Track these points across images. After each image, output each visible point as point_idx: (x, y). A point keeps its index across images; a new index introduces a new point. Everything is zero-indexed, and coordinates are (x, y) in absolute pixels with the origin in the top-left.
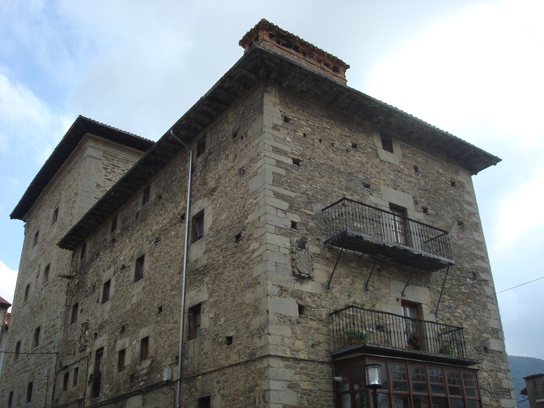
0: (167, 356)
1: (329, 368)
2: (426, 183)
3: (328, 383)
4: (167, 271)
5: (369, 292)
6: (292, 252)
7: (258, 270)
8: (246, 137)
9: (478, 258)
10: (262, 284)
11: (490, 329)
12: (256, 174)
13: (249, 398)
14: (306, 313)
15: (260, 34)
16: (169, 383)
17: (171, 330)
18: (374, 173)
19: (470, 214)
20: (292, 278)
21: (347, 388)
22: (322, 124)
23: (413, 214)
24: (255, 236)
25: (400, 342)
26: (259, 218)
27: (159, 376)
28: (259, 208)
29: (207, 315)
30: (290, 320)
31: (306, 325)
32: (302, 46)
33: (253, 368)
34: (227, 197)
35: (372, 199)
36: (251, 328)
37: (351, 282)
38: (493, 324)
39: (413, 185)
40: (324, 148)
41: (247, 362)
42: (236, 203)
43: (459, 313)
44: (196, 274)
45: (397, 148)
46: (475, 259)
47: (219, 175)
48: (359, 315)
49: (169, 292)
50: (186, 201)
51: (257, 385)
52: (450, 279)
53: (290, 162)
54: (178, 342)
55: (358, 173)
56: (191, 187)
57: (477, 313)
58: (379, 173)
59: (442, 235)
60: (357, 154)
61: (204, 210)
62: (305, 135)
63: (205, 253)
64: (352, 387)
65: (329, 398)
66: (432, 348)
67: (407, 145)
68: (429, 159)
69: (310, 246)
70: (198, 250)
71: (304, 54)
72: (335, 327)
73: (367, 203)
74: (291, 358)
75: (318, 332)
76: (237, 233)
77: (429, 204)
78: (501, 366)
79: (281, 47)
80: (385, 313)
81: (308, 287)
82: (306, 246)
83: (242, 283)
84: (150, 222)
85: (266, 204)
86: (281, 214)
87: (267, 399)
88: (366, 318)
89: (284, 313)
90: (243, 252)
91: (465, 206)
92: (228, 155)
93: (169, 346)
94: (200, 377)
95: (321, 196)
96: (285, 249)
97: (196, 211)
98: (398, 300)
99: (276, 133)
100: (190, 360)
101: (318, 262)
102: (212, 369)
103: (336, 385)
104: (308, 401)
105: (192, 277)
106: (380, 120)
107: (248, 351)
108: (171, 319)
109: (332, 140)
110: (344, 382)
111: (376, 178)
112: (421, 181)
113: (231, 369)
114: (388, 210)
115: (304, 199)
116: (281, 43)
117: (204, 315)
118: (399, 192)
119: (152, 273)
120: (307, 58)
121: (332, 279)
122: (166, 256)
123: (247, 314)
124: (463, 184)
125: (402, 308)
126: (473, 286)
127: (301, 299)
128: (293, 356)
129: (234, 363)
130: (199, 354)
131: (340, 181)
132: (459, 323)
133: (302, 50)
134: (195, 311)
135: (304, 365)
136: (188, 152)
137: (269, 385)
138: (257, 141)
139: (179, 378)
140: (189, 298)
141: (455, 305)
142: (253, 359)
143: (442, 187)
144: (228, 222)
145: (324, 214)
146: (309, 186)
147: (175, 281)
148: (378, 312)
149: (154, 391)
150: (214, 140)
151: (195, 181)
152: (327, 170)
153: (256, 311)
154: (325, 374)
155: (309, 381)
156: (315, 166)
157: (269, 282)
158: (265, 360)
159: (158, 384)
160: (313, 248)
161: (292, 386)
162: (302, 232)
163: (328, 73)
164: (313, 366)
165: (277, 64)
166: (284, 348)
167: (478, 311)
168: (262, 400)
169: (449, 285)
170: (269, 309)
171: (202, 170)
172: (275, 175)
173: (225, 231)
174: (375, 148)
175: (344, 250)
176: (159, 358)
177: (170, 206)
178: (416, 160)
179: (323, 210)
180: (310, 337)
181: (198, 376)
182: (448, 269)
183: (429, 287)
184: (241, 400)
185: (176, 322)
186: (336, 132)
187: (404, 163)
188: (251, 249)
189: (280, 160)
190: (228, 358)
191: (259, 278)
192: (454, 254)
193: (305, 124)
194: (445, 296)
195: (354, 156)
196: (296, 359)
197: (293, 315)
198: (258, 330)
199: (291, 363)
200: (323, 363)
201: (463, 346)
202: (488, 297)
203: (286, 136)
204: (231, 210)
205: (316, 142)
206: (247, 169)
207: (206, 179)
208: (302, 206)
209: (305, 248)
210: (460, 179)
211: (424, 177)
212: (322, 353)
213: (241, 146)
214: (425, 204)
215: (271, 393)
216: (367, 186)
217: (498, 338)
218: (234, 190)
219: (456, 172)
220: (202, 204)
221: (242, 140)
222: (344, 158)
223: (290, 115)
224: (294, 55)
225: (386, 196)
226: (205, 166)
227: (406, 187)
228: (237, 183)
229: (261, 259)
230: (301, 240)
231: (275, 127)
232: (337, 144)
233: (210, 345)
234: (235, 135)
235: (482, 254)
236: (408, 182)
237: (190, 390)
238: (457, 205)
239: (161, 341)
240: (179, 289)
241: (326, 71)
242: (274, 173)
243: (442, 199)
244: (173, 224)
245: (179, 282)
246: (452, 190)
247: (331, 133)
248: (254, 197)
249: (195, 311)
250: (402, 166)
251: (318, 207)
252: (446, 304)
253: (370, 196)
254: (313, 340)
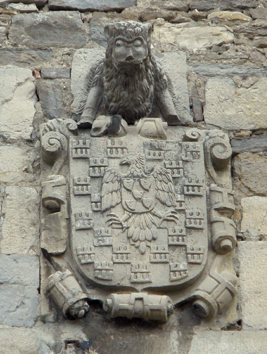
20: (45, 336)
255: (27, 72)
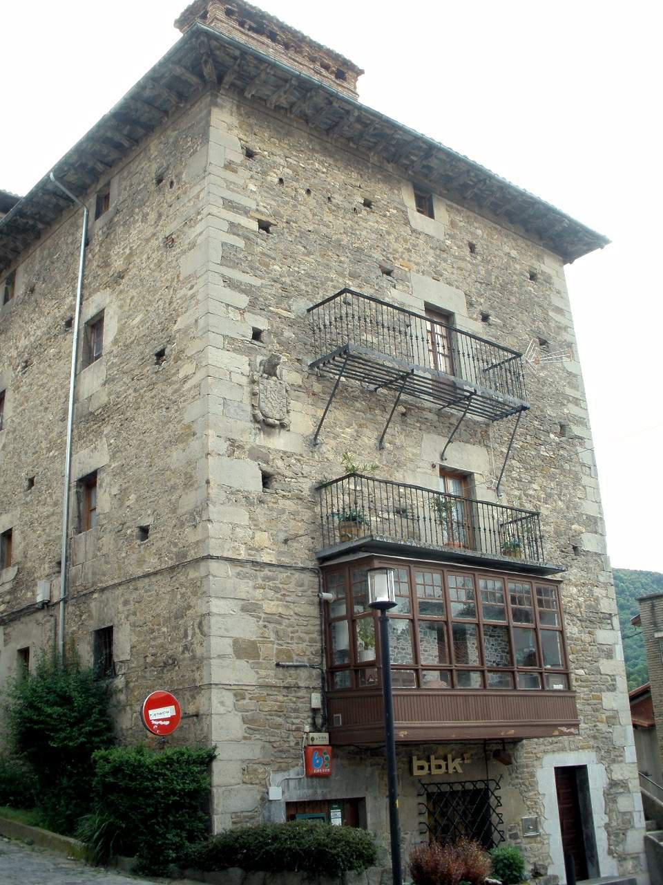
0: (42, 560)
1: (312, 579)
2: (489, 273)
3: (312, 604)
4: (43, 417)
5: (385, 452)
6: (253, 382)
7: (192, 412)
8: (178, 183)
9: (569, 401)
10: (198, 435)
11: (584, 517)
12: (193, 245)
13: (177, 628)
14: (275, 484)
15: (210, 8)
16: (46, 605)
17: (48, 517)
18: (400, 250)
19: (559, 328)
20: (252, 425)
21: (343, 611)
22: (312, 164)
23: (463, 321)
24: (189, 353)
25: (434, 536)
26: (196, 321)
27: (29, 594)
28: (197, 303)
29: (108, 489)
30: (246, 497)
31: (275, 506)
32: (284, 32)
33: (182, 579)
34: (143, 285)
35: (394, 295)
36: (180, 511)
37: (355, 434)
38: (588, 508)
39: (467, 275)
40: (315, 205)
41: (172, 568)
42: (157, 297)
43: (535, 490)
44: (90, 421)
45: (440, 210)
46: (565, 402)
47: (131, 248)
48: (365, 490)
49: (45, 452)
50: (75, 296)
51: (189, 607)
52: (522, 434)
53: (254, 226)
54: (60, 537)
55: (373, 250)
56: (83, 272)
57: (565, 491)
58: (409, 250)
59: (510, 359)
60: (372, 217)
61: (104, 310)
62: (281, 181)
63: (105, 385)
64: (350, 609)
65: (312, 628)
66: (489, 547)
67: (459, 207)
68: (494, 232)
69: (284, 372)
70: (93, 380)
71: (287, 46)
72: (324, 510)
73: (387, 300)
74: (247, 561)
75: (293, 516)
76: (158, 349)
77: (492, 307)
78: (600, 576)
79: (247, 32)
80: (411, 487)
81: (279, 442)
82: (278, 372)
83: (166, 435)
84: (15, 334)
85: (207, 297)
86: (233, 315)
87: (205, 629)
88: (378, 495)
89: (236, 486)
90: (167, 381)
91: (551, 314)
92: (148, 214)
93: (45, 544)
94: (96, 595)
95: (306, 285)
96: (239, 376)
97: (91, 312)
98: (434, 466)
99: (230, 175)
100: (80, 566)
101: (297, 399)
102: (116, 581)
103: (324, 605)
104: (277, 633)
105: (82, 425)
106: (413, 162)
107: (174, 550)
108: (48, 499)
109: (328, 191)
110: (337, 601)
111: (404, 259)
112: (481, 268)
113: (147, 580)
114: (423, 314)
115: (276, 289)
116: (247, 27)
117: (103, 490)
118: (442, 284)
119: (17, 421)
120: (291, 53)
121: (322, 428)
122: (41, 390)
123: (174, 488)
124: (550, 277)
125: (442, 480)
126: (559, 446)
127: (267, 462)
128: (251, 558)
129: (152, 570)
130: (95, 556)
131: (340, 262)
132: (535, 506)
133: (283, 39)
134: (88, 483)
135: (270, 574)
136: (80, 211)
137: (209, 607)
138: (197, 189)
139: (62, 596)
140: (78, 461)
141: (529, 478)
142: (185, 563)
143: (515, 281)
144: (144, 330)
145: (311, 318)
146: (285, 268)
147: (54, 434)
148: (399, 485)
149: (22, 619)
150: (125, 190)
151: (90, 261)
152: (318, 242)
153: (189, 482)
154: (305, 588)
155: (278, 599)
156: (298, 234)
157: (211, 432)
158: (203, 564)
159: (28, 607)
160: (289, 375)
161: (249, 608)
162: (270, 347)
163: (328, 81)
164: (285, 575)
165: (235, 58)
166: (236, 544)
167: (567, 487)
168: (197, 631)
169: (521, 443)
170: (211, 477)
171: (103, 241)
172: (225, 248)
173: (139, 345)
174: (404, 209)
175: (343, 379)
176: (29, 564)
177: (48, 305)
178: (472, 233)
179: (309, 311)
180: (280, 526)
181: (92, 593)
182: (519, 417)
183: (486, 446)
184: (164, 632)
185: (56, 504)
186: (336, 178)
187: (452, 237)
188: (181, 375)
189: (236, 222)
190: (141, 562)
191: (195, 426)
192: (531, 392)
193: (282, 162)
194: (513, 462)
195: (366, 221)
196: (257, 562)
197: (251, 489)
198: (191, 514)
199: (248, 569)
200: (303, 569)
201: (539, 544)
202: (583, 465)
203: (248, 181)
204: (149, 308)
205: (301, 194)
206: (178, 237)
207: (109, 256)
208: (273, 302)
209: (275, 375)
210: (544, 268)
211: (486, 261)
212: (302, 553)
213: (170, 197)
214: (485, 308)
215: (213, 620)
216: (388, 273)
217: (596, 532)
218: (156, 274)
219: (539, 257)
220: (101, 299)
221: (171, 187)
222: (349, 223)
223: (256, 146)
224: (268, 46)
225: (418, 291)
226: (108, 234)
227: (455, 277)
228: (160, 261)
229: (199, 392)
230: (269, 361)
231: (229, 166)
232: (338, 199)
233: (112, 542)
234: (159, 181)
235: (578, 395)
236: (458, 268)
237: (81, 616)
238: (538, 311)
239: (33, 537)
240: (62, 447)
241: (324, 76)
242: (224, 244)
243: (513, 300)
244: (51, 337)
245: (61, 434)
246: (530, 287)
247: (328, 179)
248: (189, 286)
249: (88, 483)
250: (448, 242)
251: (300, 305)
252: (514, 474)
253: (392, 290)
254: (286, 531)
255: (247, 358)
